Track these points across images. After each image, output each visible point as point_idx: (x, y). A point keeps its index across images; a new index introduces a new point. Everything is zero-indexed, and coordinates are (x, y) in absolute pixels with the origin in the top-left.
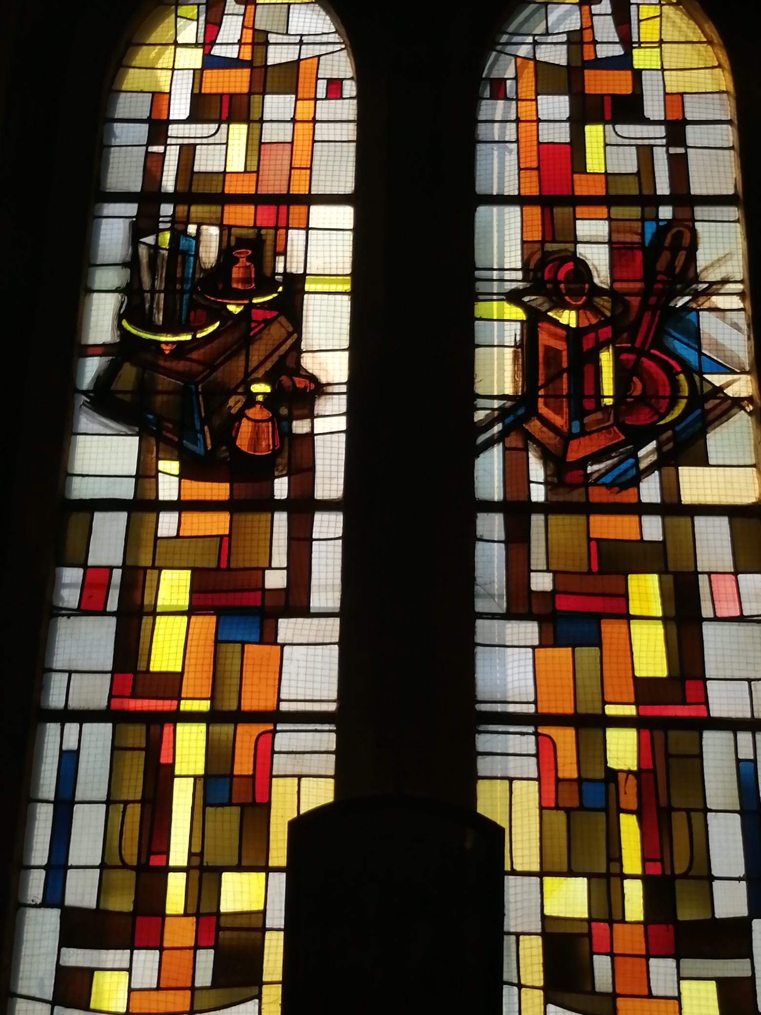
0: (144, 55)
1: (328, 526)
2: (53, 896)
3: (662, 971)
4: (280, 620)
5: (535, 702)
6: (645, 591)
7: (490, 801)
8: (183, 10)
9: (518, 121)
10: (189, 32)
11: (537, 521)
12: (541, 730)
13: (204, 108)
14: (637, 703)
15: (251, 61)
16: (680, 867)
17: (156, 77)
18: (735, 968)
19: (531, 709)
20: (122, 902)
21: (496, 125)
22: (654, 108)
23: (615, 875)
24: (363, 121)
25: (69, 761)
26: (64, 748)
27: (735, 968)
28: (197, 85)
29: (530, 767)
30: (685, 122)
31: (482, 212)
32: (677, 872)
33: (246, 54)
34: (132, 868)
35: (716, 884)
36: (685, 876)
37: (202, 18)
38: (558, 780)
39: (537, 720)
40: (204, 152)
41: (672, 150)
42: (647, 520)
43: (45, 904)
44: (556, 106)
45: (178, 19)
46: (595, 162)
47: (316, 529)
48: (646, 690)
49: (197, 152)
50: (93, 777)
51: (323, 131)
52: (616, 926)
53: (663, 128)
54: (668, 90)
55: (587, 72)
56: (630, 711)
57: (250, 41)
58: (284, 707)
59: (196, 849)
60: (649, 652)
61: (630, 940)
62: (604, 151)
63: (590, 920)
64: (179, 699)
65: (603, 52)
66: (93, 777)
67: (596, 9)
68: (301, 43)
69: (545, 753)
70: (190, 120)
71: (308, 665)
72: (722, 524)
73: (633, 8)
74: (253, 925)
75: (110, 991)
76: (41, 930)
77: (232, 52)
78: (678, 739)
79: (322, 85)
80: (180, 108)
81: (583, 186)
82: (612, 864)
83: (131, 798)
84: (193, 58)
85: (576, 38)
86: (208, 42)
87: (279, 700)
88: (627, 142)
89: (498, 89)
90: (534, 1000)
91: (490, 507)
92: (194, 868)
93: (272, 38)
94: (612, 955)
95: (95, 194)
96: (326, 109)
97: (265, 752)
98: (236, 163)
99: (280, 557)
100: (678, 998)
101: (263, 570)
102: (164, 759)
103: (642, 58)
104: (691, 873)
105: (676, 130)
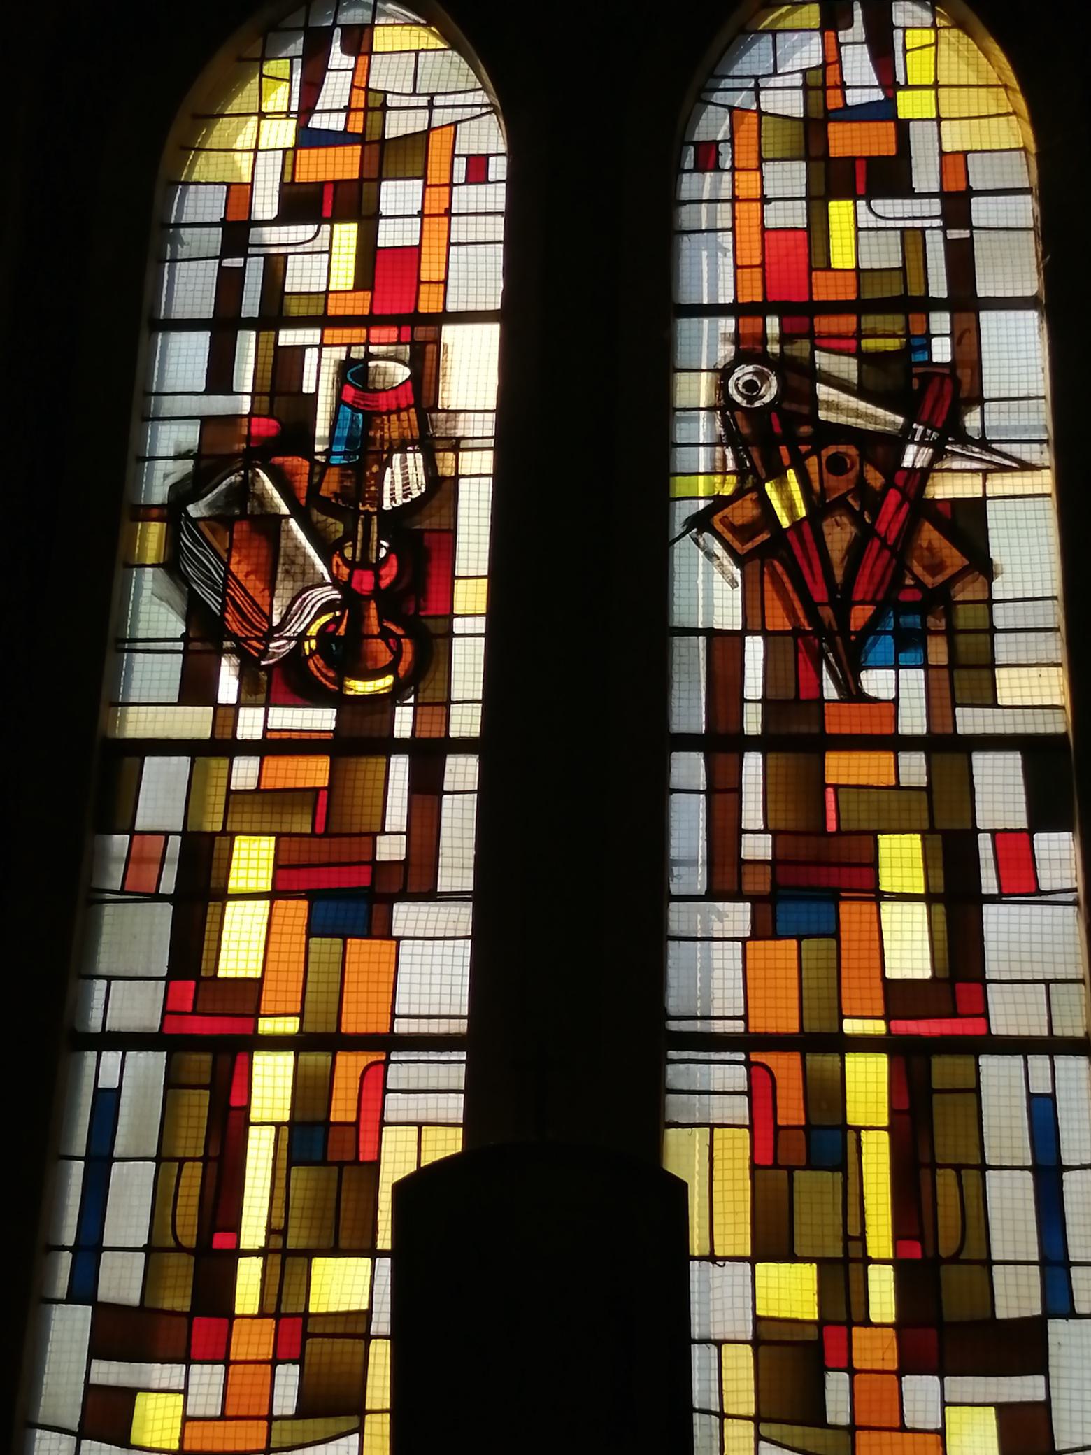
0: (221, 132)
1: (462, 772)
2: (83, 1289)
3: (920, 1394)
4: (396, 907)
5: (745, 1018)
6: (902, 860)
7: (684, 1154)
8: (271, 67)
9: (734, 200)
10: (279, 97)
11: (753, 763)
12: (755, 1057)
13: (301, 203)
14: (887, 1018)
15: (363, 135)
16: (946, 1247)
17: (234, 162)
18: (1025, 1388)
19: (739, 1026)
20: (178, 1299)
21: (704, 206)
22: (925, 176)
23: (855, 1260)
24: (513, 215)
25: (107, 1102)
26: (100, 1086)
27: (1025, 1388)
28: (289, 169)
29: (739, 1109)
30: (971, 192)
31: (685, 326)
32: (944, 1253)
33: (357, 126)
34: (188, 1251)
35: (996, 1269)
36: (955, 1259)
37: (297, 76)
38: (777, 1129)
39: (749, 1043)
40: (298, 265)
41: (954, 234)
42: (904, 758)
43: (72, 1298)
44: (788, 178)
45: (264, 79)
46: (842, 255)
47: (448, 777)
48: (900, 997)
49: (289, 266)
50: (137, 1124)
51: (461, 228)
52: (856, 1331)
53: (937, 201)
54: (947, 147)
55: (832, 127)
56: (877, 1027)
57: (362, 105)
58: (401, 1027)
59: (278, 1223)
60: (907, 943)
61: (874, 1348)
62: (855, 236)
63: (821, 1324)
64: (257, 1015)
65: (854, 97)
66: (137, 1124)
67: (843, 36)
68: (431, 107)
69: (760, 1090)
70: (303, 348)
71: (431, 966)
72: (1012, 762)
73: (898, 34)
74: (354, 1326)
75: (157, 1420)
76: (69, 1328)
77: (336, 123)
78: (944, 1069)
79: (460, 166)
80: (266, 204)
81: (825, 289)
82: (851, 1244)
83: (189, 1154)
84: (283, 133)
85: (815, 79)
86: (308, 107)
87: (394, 1016)
88: (891, 224)
89: (708, 158)
90: (740, 1435)
91: (688, 742)
92: (275, 1251)
93: (392, 101)
94: (852, 1372)
95: (146, 322)
96: (466, 197)
97: (374, 1087)
98: (344, 277)
99: (397, 815)
100: (942, 1432)
101: (373, 835)
102: (235, 1101)
103: (909, 105)
104: (963, 1257)
105: (956, 205)
